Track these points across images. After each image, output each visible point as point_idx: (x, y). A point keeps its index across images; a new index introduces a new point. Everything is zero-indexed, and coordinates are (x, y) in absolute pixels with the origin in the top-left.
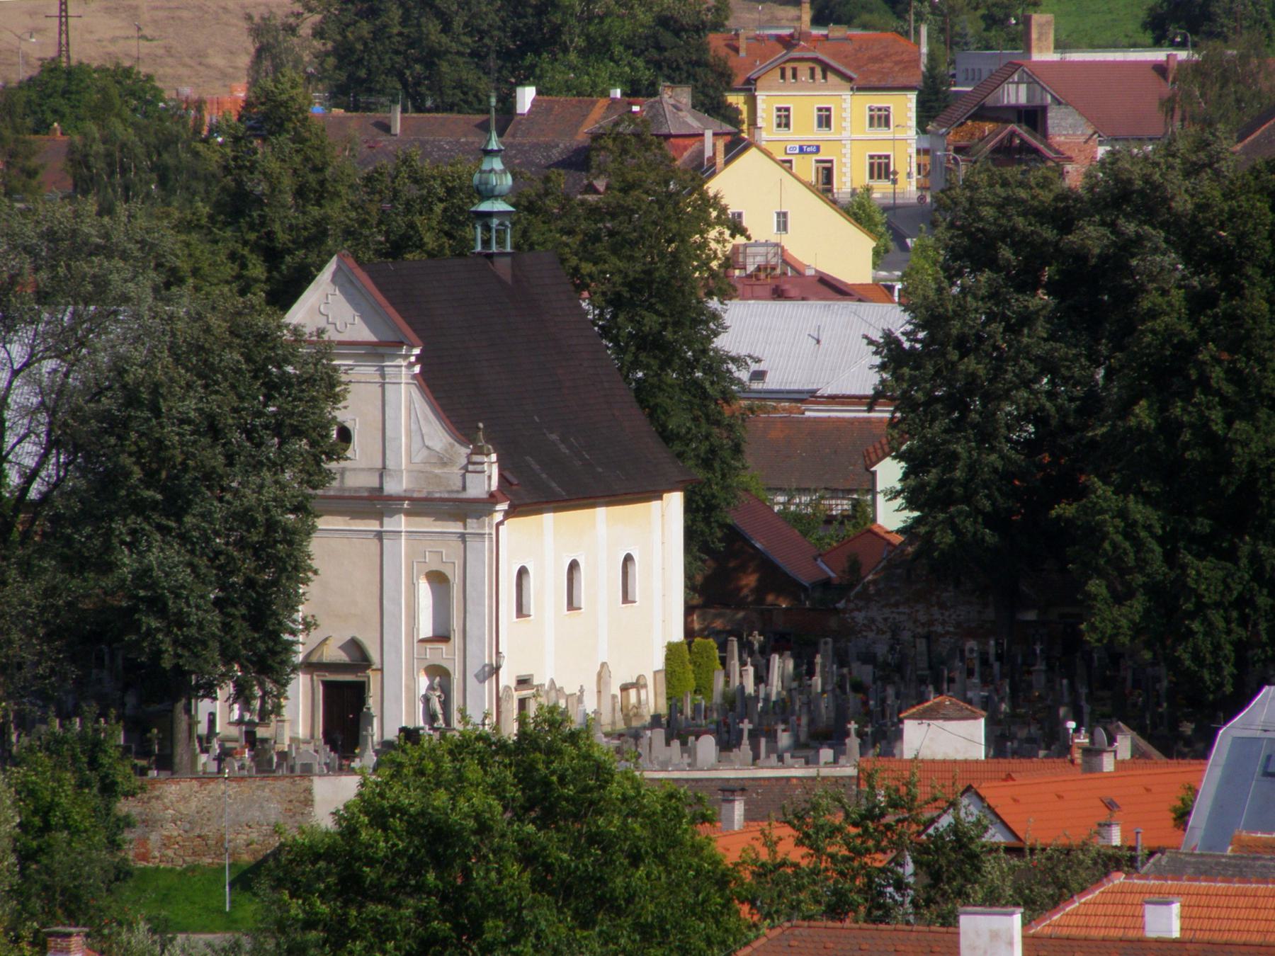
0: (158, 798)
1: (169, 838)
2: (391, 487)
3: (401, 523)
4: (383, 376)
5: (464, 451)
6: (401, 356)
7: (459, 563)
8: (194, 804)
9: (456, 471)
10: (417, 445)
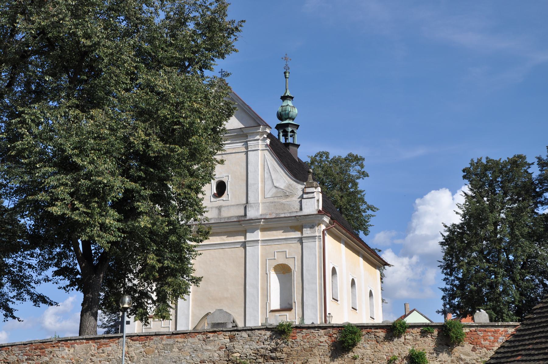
2: (252, 214)
3: (258, 235)
4: (247, 148)
5: (299, 187)
6: (258, 133)
7: (298, 257)
9: (295, 200)
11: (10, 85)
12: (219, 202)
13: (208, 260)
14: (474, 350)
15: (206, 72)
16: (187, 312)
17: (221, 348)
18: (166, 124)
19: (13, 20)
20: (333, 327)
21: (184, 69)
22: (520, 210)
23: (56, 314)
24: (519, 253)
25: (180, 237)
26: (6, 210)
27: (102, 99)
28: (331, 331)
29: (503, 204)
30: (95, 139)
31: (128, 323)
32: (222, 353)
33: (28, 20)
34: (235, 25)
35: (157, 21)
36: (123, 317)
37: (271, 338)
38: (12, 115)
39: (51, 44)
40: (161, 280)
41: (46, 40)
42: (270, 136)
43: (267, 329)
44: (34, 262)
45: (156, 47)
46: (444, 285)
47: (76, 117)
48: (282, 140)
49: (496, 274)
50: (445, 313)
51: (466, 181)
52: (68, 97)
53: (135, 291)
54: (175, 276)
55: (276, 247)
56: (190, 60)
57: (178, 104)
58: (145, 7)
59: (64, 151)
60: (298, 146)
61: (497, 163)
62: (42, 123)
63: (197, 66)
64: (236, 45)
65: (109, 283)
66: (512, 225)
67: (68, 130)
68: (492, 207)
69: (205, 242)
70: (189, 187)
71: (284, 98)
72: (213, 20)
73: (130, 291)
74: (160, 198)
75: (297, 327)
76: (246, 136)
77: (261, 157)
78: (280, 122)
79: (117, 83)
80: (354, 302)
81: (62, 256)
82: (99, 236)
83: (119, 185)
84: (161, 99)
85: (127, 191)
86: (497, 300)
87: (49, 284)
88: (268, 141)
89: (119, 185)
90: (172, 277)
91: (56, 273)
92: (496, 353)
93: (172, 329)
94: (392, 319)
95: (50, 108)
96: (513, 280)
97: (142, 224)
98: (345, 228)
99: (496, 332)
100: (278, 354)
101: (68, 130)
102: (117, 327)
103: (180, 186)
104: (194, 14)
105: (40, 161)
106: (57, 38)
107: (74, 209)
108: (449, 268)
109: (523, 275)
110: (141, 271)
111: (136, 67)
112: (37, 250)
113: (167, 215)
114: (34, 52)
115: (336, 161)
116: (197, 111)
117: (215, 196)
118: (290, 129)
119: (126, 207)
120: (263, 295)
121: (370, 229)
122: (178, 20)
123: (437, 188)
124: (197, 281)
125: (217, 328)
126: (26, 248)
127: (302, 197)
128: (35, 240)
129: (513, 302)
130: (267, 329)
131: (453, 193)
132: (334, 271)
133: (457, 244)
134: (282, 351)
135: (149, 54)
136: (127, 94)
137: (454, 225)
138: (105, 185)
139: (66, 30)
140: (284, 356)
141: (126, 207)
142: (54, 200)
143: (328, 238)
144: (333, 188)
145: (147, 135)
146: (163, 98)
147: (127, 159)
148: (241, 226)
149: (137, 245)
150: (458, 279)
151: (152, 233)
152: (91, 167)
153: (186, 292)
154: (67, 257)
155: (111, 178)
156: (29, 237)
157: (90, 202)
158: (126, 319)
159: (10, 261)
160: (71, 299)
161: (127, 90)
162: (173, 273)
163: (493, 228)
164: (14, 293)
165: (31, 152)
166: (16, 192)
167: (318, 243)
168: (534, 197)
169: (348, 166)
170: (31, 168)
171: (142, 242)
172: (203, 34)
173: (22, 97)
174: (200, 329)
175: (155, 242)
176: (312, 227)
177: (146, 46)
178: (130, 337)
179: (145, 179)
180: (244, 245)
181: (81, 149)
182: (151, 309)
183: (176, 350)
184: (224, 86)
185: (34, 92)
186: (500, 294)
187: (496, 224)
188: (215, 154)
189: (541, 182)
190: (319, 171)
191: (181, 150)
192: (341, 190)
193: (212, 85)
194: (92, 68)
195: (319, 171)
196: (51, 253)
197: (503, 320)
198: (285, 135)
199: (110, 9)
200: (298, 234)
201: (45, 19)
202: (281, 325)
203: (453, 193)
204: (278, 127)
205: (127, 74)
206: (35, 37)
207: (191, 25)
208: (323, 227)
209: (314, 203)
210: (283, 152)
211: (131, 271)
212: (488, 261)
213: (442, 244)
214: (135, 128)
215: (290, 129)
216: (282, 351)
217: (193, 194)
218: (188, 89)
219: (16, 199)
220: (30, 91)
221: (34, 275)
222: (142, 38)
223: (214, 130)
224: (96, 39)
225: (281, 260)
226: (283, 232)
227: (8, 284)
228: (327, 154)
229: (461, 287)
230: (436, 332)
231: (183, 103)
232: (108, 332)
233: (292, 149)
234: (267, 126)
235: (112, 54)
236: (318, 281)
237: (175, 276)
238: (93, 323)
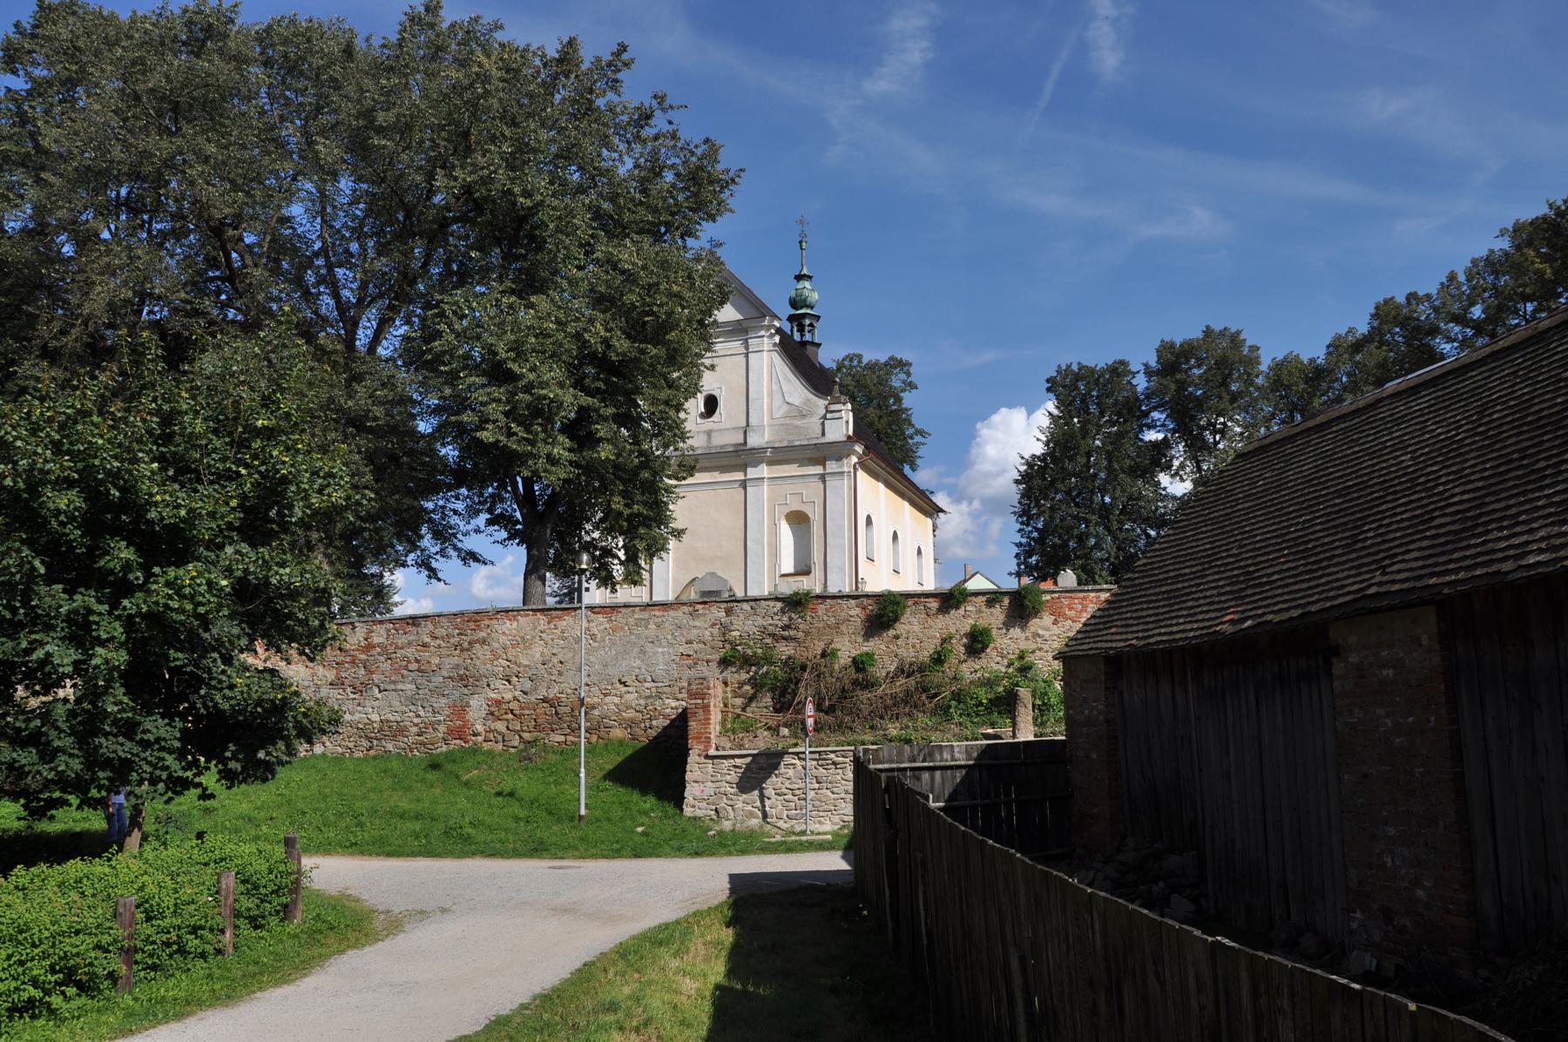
0: (484, 642)
1: (498, 703)
2: (754, 441)
3: (764, 471)
4: (747, 348)
5: (821, 403)
6: (762, 328)
7: (819, 502)
8: (537, 651)
9: (815, 421)
10: (778, 402)
11: (425, 265)
12: (708, 424)
13: (695, 506)
14: (1055, 622)
15: (690, 242)
16: (667, 575)
17: (713, 625)
18: (634, 314)
19: (431, 177)
20: (867, 596)
21: (658, 238)
22: (1120, 435)
23: (489, 577)
24: (1118, 493)
25: (655, 473)
26: (423, 436)
27: (544, 280)
28: (865, 601)
29: (1099, 427)
30: (536, 336)
31: (587, 590)
32: (715, 631)
33: (450, 176)
34: (731, 174)
35: (622, 171)
36: (580, 582)
37: (783, 611)
38: (427, 306)
39: (478, 207)
40: (630, 534)
41: (472, 202)
42: (779, 331)
43: (777, 599)
44: (460, 506)
45: (620, 207)
46: (1018, 538)
47: (511, 306)
48: (797, 337)
49: (1087, 522)
50: (1019, 575)
51: (1051, 395)
52: (500, 279)
53: (596, 548)
54: (649, 527)
55: (788, 488)
56: (668, 225)
57: (650, 286)
58: (605, 152)
59: (495, 354)
60: (819, 345)
61: (1092, 371)
62: (465, 316)
63: (678, 233)
64: (732, 203)
65: (561, 537)
66: (1110, 457)
67: (501, 325)
68: (1084, 432)
69: (690, 481)
70: (667, 403)
71: (799, 278)
72: (700, 168)
73: (589, 546)
74: (627, 419)
75: (818, 597)
76: (746, 331)
77: (767, 361)
78: (794, 312)
79: (567, 257)
80: (896, 562)
81: (496, 498)
82: (545, 471)
83: (570, 400)
84: (627, 280)
85: (582, 410)
86: (1087, 556)
87: (481, 537)
88: (777, 339)
89: (570, 400)
90: (646, 527)
91: (489, 522)
92: (1085, 625)
93: (646, 599)
94: (947, 586)
95: (476, 295)
96: (1109, 531)
97: (603, 455)
98: (884, 459)
99: (1084, 598)
100: (792, 633)
101: (501, 325)
102: (572, 595)
103: (654, 401)
104: (674, 160)
105: (464, 368)
106: (486, 199)
107: (510, 434)
108: (1025, 515)
109: (1121, 523)
110: (602, 520)
111: (592, 236)
112: (464, 491)
113: (637, 443)
114: (456, 220)
115: (873, 366)
116: (678, 296)
117: (703, 416)
118: (807, 322)
119: (580, 431)
120: (770, 553)
121: (918, 462)
122: (652, 170)
123: (1011, 406)
124: (678, 534)
125: (709, 598)
126: (450, 488)
127: (824, 417)
128: (461, 477)
129: (1107, 560)
130: (777, 599)
131: (1030, 413)
132: (869, 521)
133: (1037, 482)
134: (797, 629)
135: (611, 217)
136: (581, 274)
137: (1034, 456)
138: (552, 401)
139: (499, 186)
140: (801, 635)
141: (580, 431)
142: (484, 420)
143: (861, 474)
144: (868, 405)
145: (607, 330)
146: (630, 278)
147: (581, 364)
148: (739, 458)
149: (597, 484)
150: (1037, 530)
151: (616, 466)
152: (532, 376)
153: (664, 548)
154: (502, 500)
155: (559, 392)
156: (453, 472)
157: (531, 425)
158: (585, 585)
159: (430, 505)
160: (510, 559)
161: (580, 268)
162: (647, 522)
163: (1084, 460)
164: (437, 548)
165: (452, 356)
166: (434, 411)
167: (846, 482)
168: (1139, 418)
169: (889, 373)
170: (452, 378)
171: (602, 479)
172: (686, 188)
173: (441, 282)
174: (684, 598)
175: (620, 479)
176: (839, 459)
177: (606, 205)
178: (591, 608)
179: (605, 392)
180: (744, 484)
181: (518, 350)
182: (618, 571)
183: (652, 626)
184: (714, 261)
185: (456, 273)
186: (1092, 549)
187: (1089, 455)
188: (702, 357)
189: (1148, 397)
190: (848, 380)
191: (654, 351)
192: (879, 406)
193: (698, 259)
194: (532, 238)
195: (848, 380)
196: (481, 495)
197: (1095, 583)
198: (801, 330)
199: (557, 156)
200: (819, 470)
201: (471, 173)
202: (796, 594)
203: (1030, 413)
204: (791, 318)
205: (581, 246)
206: (458, 199)
207: (669, 177)
208: (854, 459)
209: (842, 425)
210: (798, 354)
211: (588, 520)
212: (1077, 505)
213: (1017, 482)
214: (591, 321)
215: (807, 322)
216: (797, 629)
217: (672, 413)
218: (664, 265)
219: (435, 421)
220: (450, 273)
221: (462, 524)
222: (600, 195)
223: (701, 322)
224: (539, 198)
225: (796, 506)
226: (1452, 277)
227: (429, 536)
228: (860, 357)
229: (1041, 540)
230: (1006, 601)
231: (658, 284)
232: (560, 602)
233: (810, 349)
234: (775, 317)
235: (559, 218)
236: (847, 534)
237: (649, 527)
238: (540, 590)
